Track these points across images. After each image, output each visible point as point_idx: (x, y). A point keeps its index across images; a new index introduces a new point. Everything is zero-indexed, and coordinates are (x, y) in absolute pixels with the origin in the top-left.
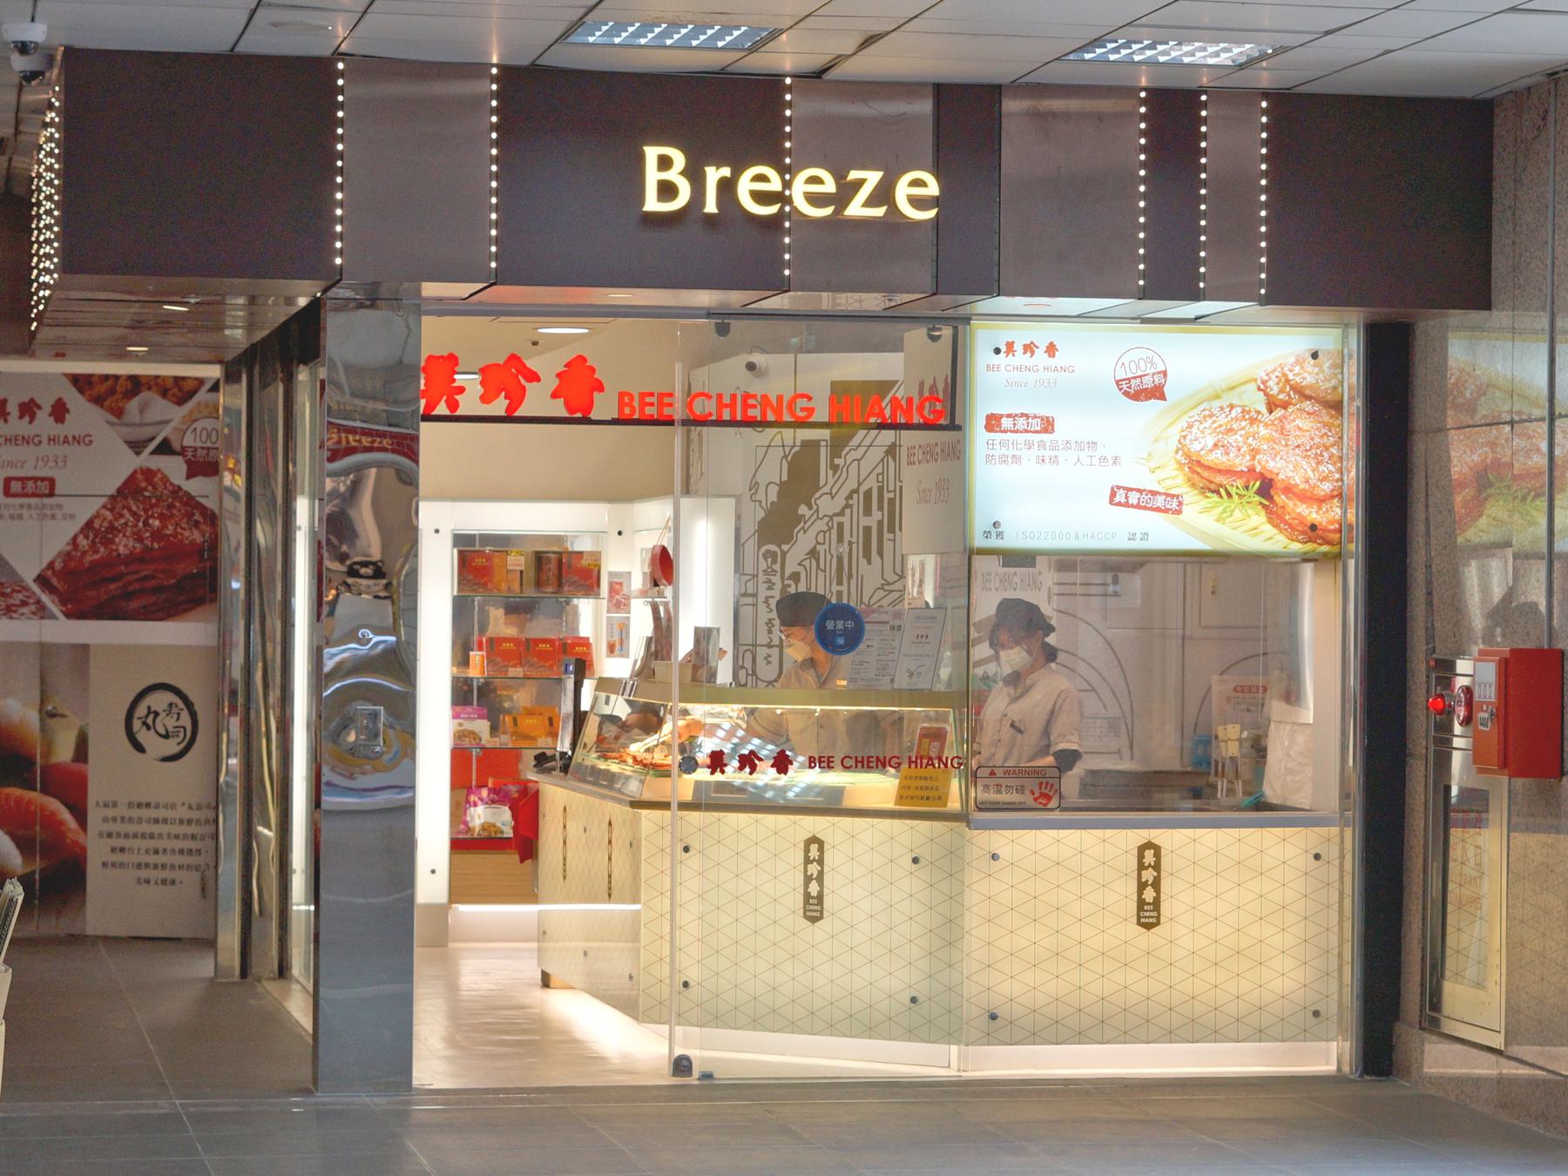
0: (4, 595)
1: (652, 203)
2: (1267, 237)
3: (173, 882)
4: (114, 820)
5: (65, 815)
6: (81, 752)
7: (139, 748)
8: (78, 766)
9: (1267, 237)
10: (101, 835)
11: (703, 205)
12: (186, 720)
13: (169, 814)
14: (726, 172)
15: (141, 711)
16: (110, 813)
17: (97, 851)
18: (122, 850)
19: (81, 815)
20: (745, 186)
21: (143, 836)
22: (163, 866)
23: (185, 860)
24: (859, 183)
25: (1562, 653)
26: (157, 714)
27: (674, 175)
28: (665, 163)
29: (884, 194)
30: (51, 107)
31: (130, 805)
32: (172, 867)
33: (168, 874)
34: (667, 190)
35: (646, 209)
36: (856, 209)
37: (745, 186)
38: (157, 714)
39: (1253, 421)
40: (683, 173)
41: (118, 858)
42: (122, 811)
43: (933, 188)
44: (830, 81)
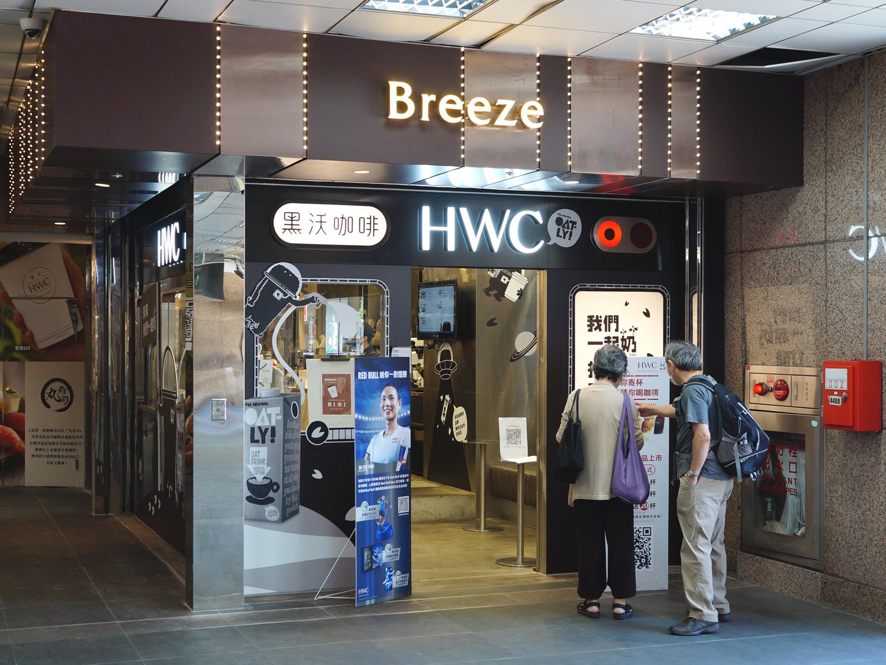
1: (394, 114)
2: (700, 151)
3: (63, 463)
4: (37, 437)
5: (15, 435)
6: (22, 407)
7: (48, 406)
8: (21, 414)
10: (656, 392)
11: (421, 116)
12: (68, 394)
13: (62, 434)
14: (433, 97)
15: (48, 390)
16: (35, 433)
17: (29, 450)
18: (40, 449)
19: (22, 436)
20: (443, 107)
21: (50, 443)
22: (59, 456)
23: (69, 453)
25: (880, 365)
26: (55, 391)
27: (406, 98)
28: (400, 91)
31: (44, 430)
32: (63, 456)
33: (61, 460)
34: (402, 107)
35: (390, 117)
36: (501, 121)
38: (55, 391)
40: (410, 97)
41: (39, 453)
42: (40, 433)
43: (540, 111)
44: (484, 52)
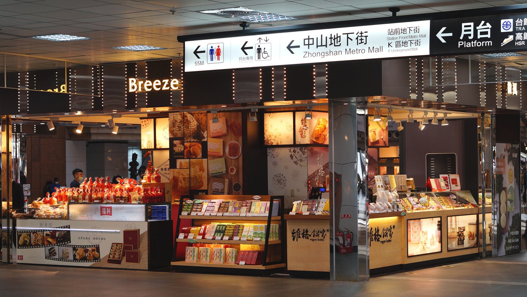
0: (507, 125)
9: (183, 97)
14: (142, 82)
24: (164, 83)
27: (134, 84)
28: (133, 81)
29: (168, 85)
30: (316, 75)
34: (133, 87)
37: (146, 85)
39: (300, 160)
